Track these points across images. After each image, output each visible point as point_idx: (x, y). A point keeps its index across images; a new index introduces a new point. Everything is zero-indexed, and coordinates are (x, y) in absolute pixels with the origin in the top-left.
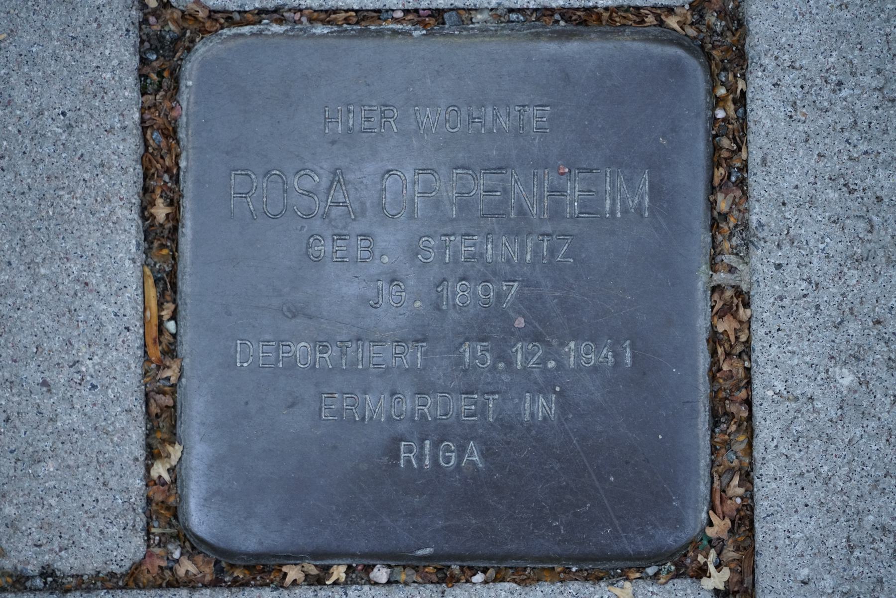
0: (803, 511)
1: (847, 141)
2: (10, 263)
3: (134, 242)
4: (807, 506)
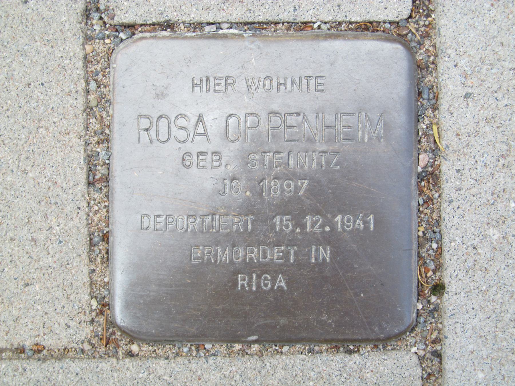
0: (472, 312)
1: (496, 98)
2: (12, 171)
3: (82, 158)
4: (473, 309)
